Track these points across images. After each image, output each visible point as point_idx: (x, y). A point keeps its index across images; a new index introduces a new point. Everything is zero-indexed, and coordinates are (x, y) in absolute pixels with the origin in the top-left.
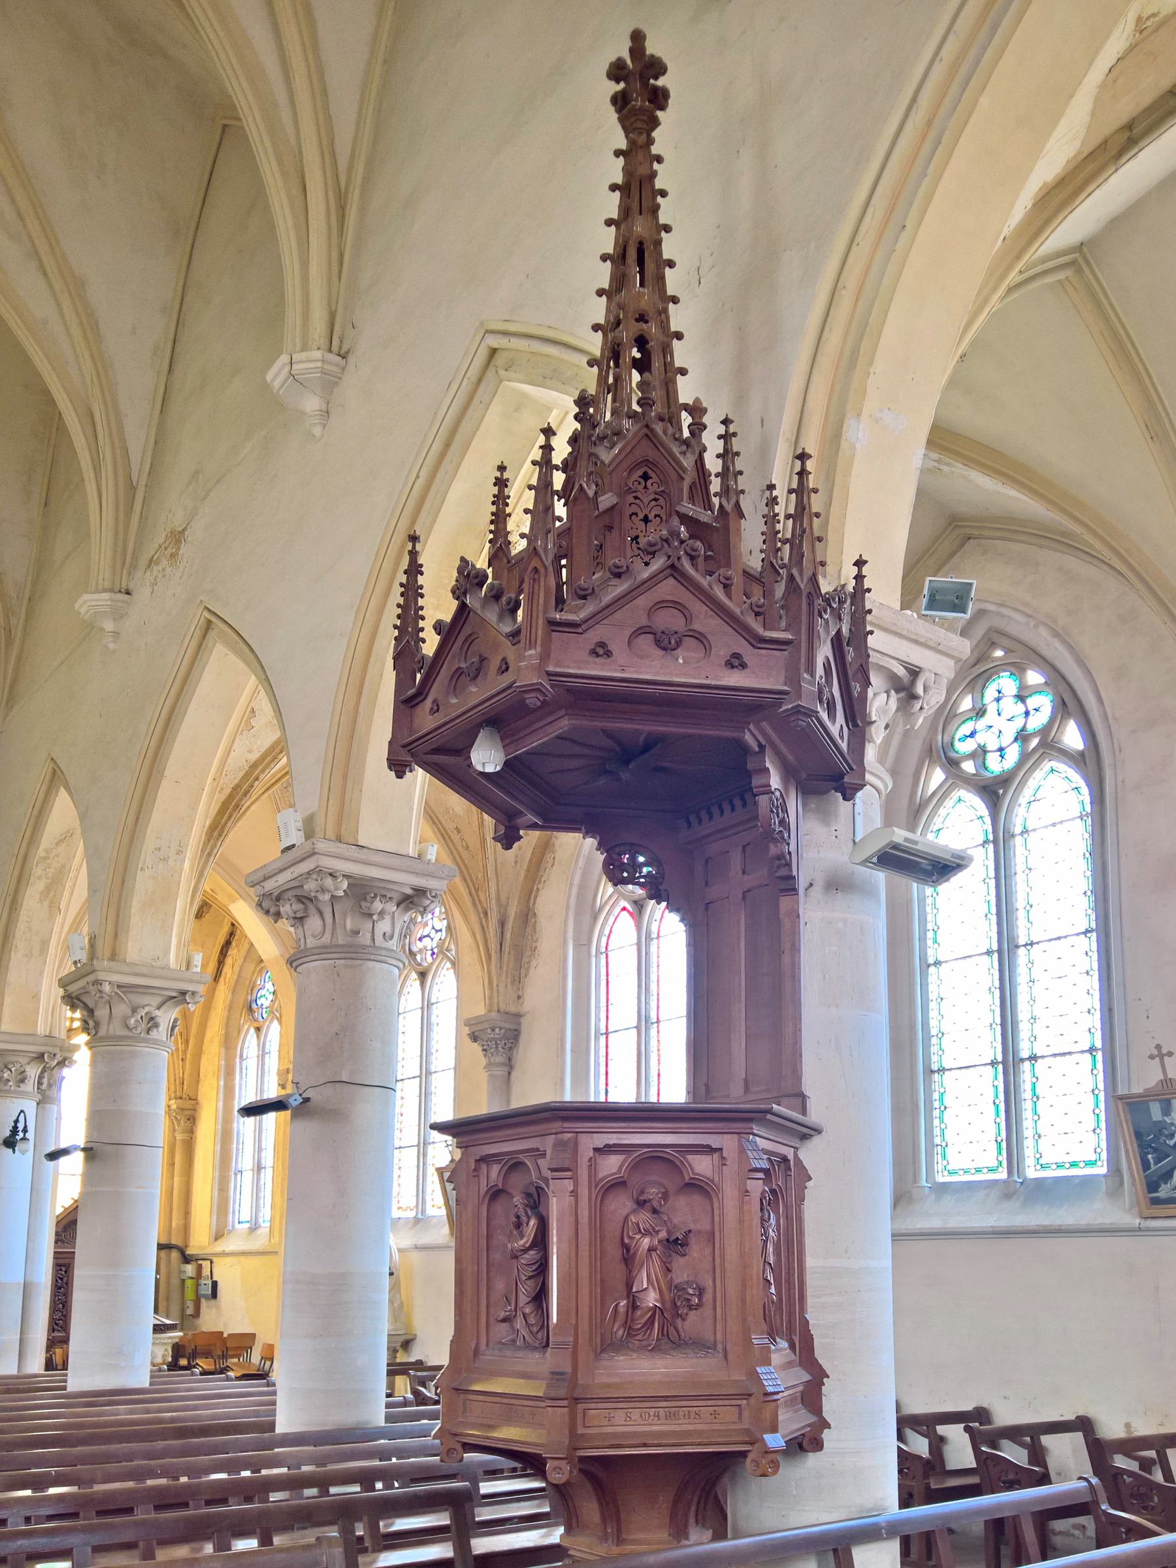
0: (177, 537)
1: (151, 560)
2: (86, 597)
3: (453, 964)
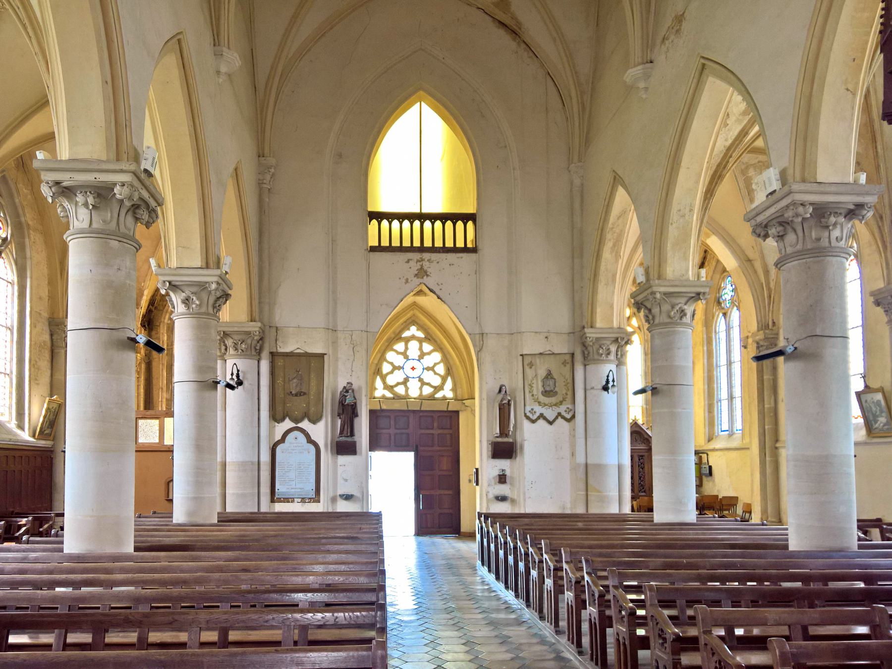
0: (680, 19)
1: (664, 39)
2: (630, 71)
3: (856, 256)
